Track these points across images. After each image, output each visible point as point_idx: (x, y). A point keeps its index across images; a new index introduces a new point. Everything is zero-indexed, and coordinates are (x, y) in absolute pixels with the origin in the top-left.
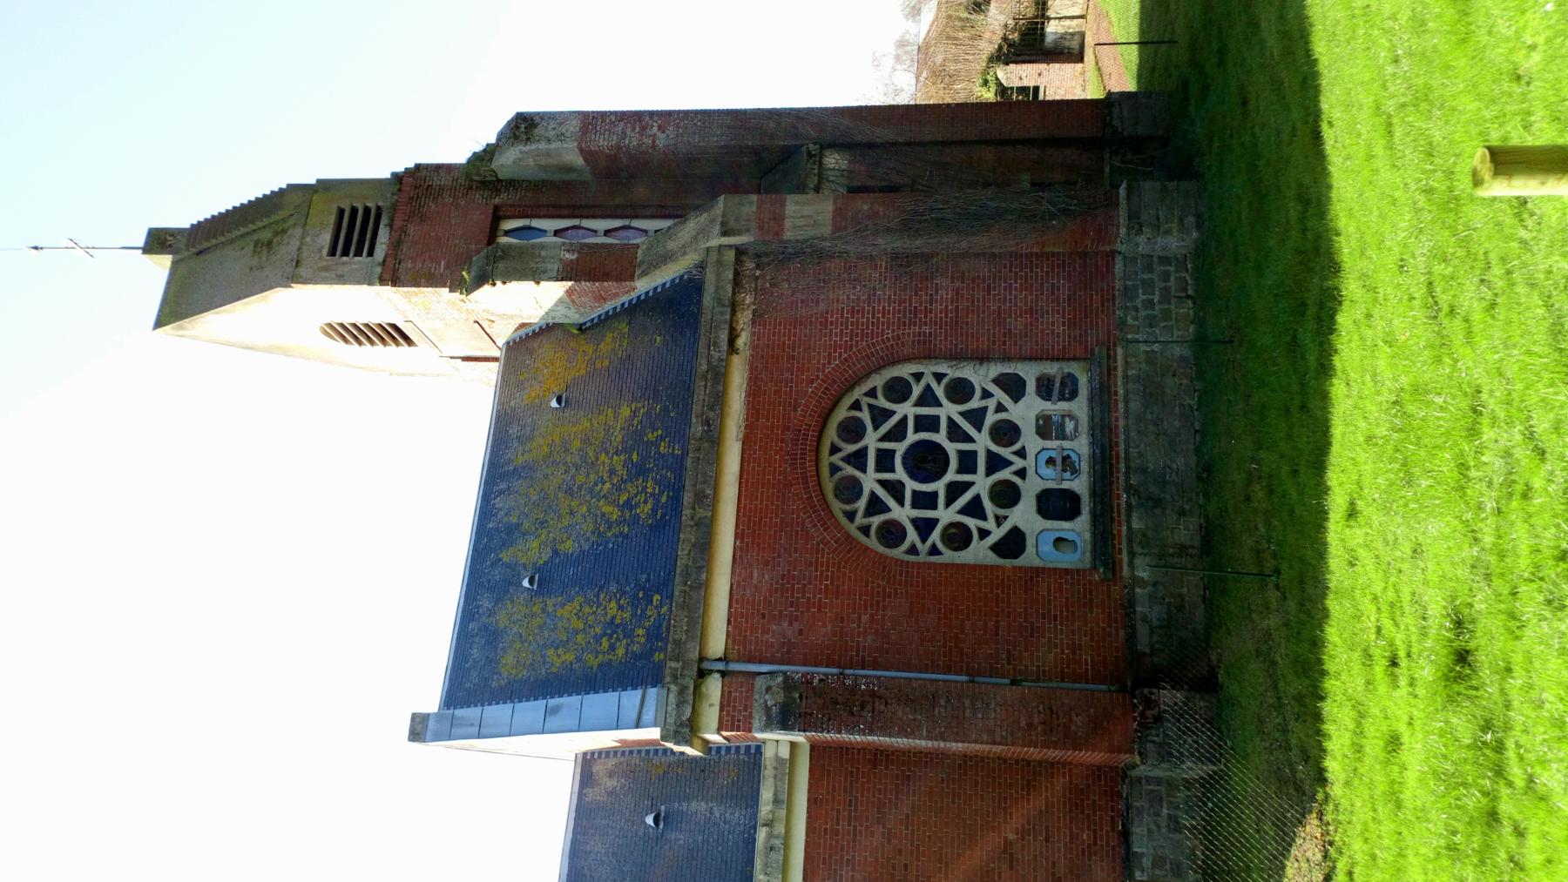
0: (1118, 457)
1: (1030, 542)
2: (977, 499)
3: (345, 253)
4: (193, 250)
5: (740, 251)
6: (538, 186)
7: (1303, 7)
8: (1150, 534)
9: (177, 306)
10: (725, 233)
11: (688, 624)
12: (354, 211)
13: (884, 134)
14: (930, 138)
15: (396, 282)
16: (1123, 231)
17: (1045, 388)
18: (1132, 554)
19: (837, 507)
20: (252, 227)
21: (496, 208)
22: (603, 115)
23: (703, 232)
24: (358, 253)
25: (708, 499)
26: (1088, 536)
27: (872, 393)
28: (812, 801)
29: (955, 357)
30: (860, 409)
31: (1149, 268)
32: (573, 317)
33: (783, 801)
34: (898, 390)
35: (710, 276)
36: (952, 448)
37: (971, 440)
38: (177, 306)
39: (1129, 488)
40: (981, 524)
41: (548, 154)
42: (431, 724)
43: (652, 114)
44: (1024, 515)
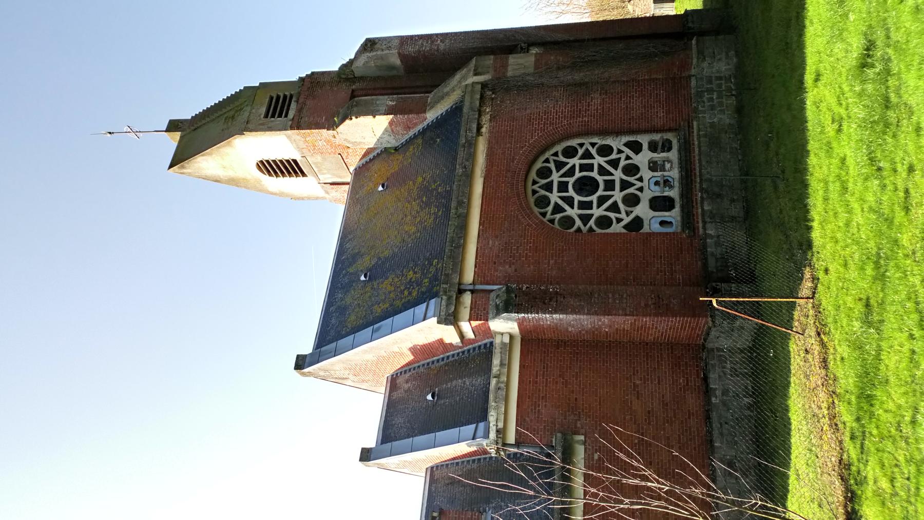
1: (646, 223)
2: (615, 203)
3: (273, 116)
4: (193, 128)
5: (484, 85)
6: (375, 79)
7: (805, 4)
8: (714, 212)
9: (178, 160)
10: (476, 74)
12: (278, 97)
13: (559, 37)
14: (587, 37)
15: (299, 127)
17: (653, 147)
18: (704, 223)
19: (536, 210)
20: (224, 111)
22: (411, 37)
23: (464, 78)
24: (280, 116)
25: (465, 204)
26: (679, 218)
27: (556, 154)
28: (522, 367)
29: (603, 133)
31: (710, 81)
32: (393, 142)
33: (506, 364)
34: (570, 152)
36: (600, 179)
37: (612, 174)
39: (702, 190)
40: (618, 215)
41: (382, 58)
42: (307, 360)
43: (437, 35)
44: (642, 210)
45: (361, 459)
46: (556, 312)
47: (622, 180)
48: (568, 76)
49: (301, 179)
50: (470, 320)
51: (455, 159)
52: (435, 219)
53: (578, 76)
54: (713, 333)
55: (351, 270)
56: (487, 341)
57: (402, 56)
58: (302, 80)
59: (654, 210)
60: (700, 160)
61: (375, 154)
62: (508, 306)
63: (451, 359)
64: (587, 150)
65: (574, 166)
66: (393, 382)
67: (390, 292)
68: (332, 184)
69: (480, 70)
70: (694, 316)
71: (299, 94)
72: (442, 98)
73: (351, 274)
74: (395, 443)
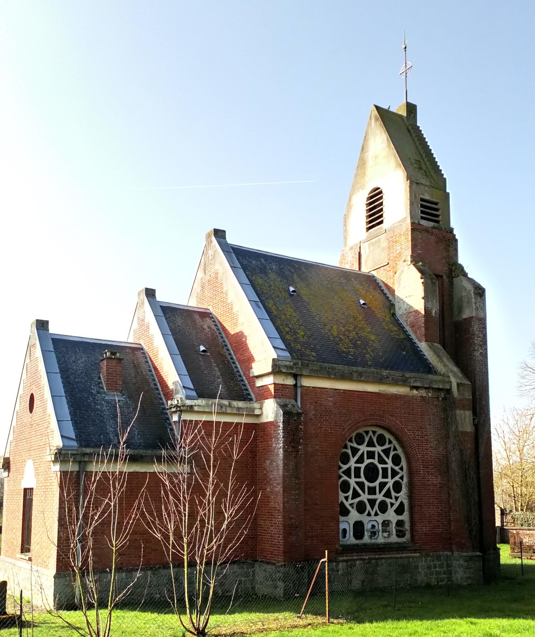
0: (381, 555)
2: (359, 495)
3: (422, 206)
4: (410, 128)
5: (449, 391)
6: (451, 296)
9: (385, 116)
10: (458, 384)
11: (315, 370)
13: (482, 449)
14: (481, 471)
16: (465, 554)
17: (400, 523)
18: (347, 561)
19: (354, 435)
20: (426, 159)
21: (442, 276)
22: (485, 328)
23: (455, 375)
24: (422, 212)
25: (360, 378)
26: (348, 543)
27: (395, 449)
29: (411, 485)
30: (389, 444)
32: (399, 312)
33: (239, 412)
34: (396, 460)
35: (435, 378)
36: (376, 484)
38: (385, 116)
40: (350, 497)
41: (469, 302)
42: (222, 240)
43: (486, 349)
45: (147, 290)
46: (285, 451)
47: (375, 500)
48: (454, 457)
49: (365, 226)
50: (275, 384)
51: (392, 369)
52: (344, 352)
53: (454, 466)
54: (269, 568)
55: (295, 277)
56: (253, 396)
57: (470, 320)
58: (452, 230)
59: (354, 525)
60: (392, 558)
61: (388, 295)
62: (288, 415)
63: (233, 365)
64: (398, 473)
65: (386, 463)
66: (206, 315)
67: (285, 314)
68: (360, 253)
69: (461, 388)
70: (284, 552)
71: (439, 229)
72: (438, 356)
73: (292, 277)
74: (164, 318)
